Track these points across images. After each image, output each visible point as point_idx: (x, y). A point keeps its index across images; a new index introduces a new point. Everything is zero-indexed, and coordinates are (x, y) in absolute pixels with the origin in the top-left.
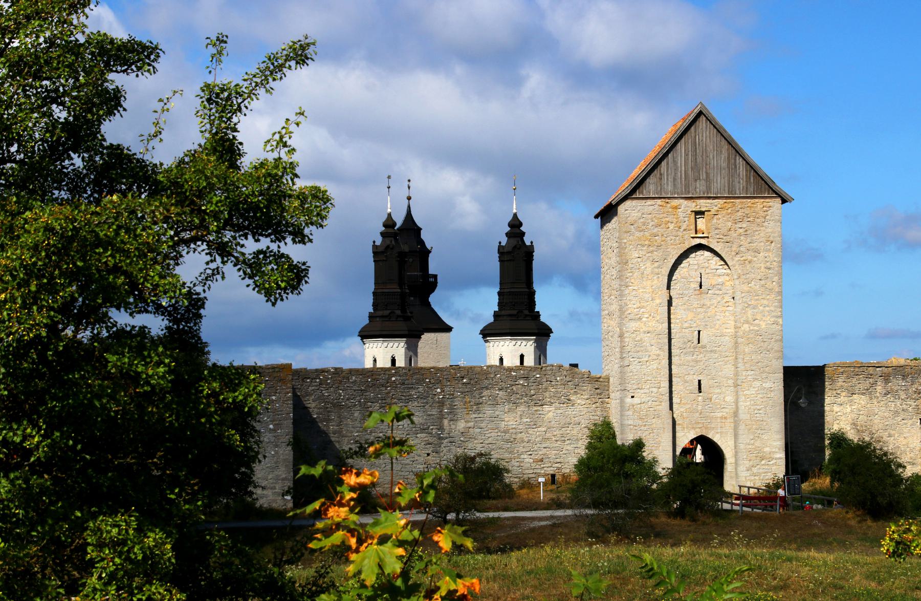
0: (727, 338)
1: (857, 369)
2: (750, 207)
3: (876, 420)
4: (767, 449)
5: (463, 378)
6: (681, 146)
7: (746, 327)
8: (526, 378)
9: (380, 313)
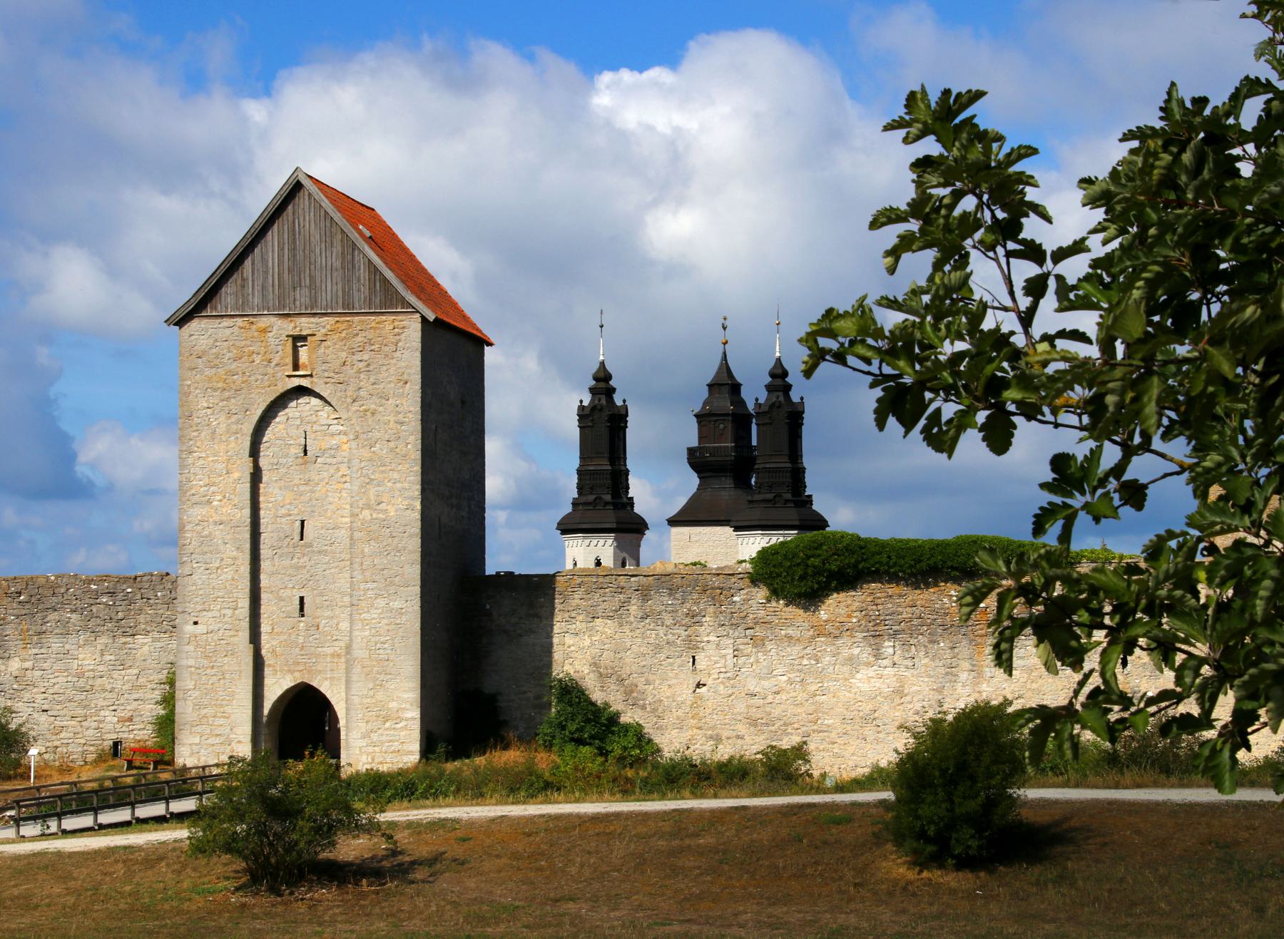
0: (343, 531)
1: (601, 580)
2: (375, 328)
3: (629, 658)
4: (393, 705)
5: (20, 594)
6: (273, 236)
7: (366, 514)
8: (112, 594)
9: (583, 499)
